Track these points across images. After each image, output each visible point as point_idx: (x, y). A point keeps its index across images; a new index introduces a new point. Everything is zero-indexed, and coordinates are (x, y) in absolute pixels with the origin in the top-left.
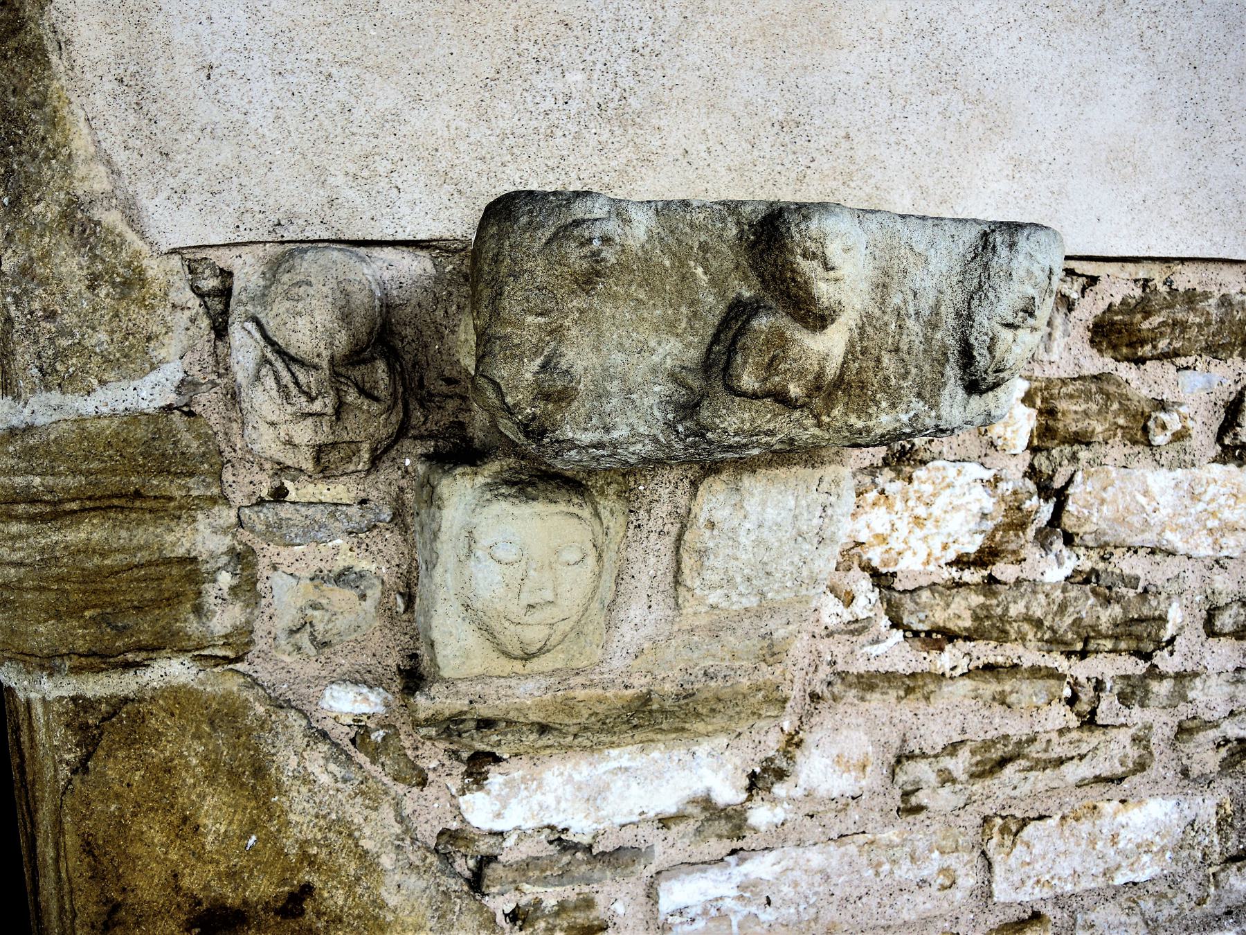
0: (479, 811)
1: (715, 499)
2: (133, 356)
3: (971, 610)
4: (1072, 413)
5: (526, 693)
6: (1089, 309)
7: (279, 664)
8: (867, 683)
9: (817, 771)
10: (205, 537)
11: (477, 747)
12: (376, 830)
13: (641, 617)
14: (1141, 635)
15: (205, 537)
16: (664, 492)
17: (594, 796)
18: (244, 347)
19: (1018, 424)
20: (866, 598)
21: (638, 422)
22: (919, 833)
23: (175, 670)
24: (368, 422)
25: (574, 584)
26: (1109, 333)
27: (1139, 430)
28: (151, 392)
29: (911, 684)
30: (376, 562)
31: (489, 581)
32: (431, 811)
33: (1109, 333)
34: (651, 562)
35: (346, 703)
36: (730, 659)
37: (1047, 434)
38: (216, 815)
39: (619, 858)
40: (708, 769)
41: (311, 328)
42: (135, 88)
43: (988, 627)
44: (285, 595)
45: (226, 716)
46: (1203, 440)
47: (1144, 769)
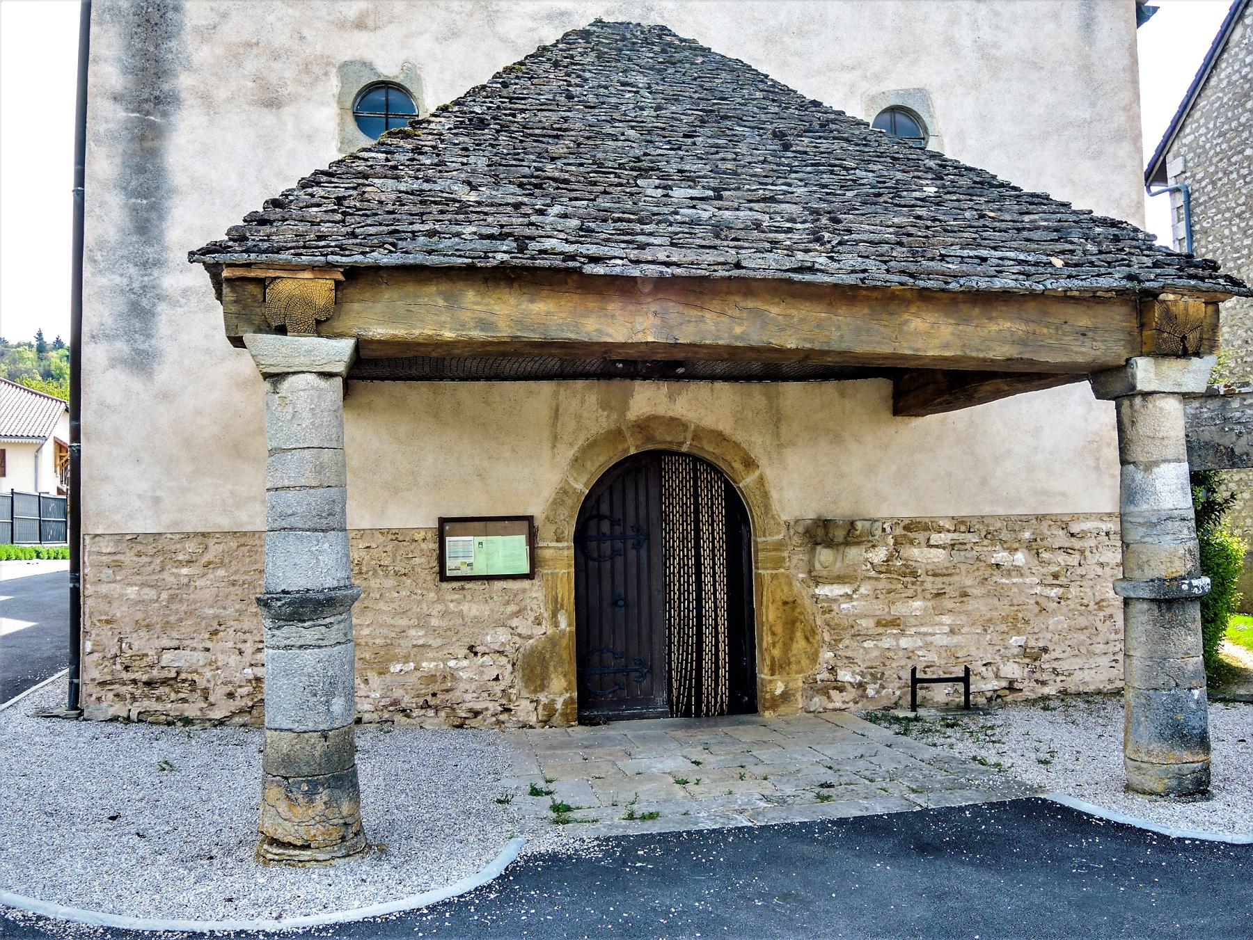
0: (817, 591)
1: (847, 550)
2: (778, 533)
3: (885, 568)
4: (900, 540)
5: (825, 573)
6: (902, 525)
7: (793, 571)
8: (870, 578)
9: (863, 590)
10: (786, 554)
11: (817, 581)
12: (804, 593)
13: (838, 564)
14: (914, 574)
15: (786, 554)
16: (841, 548)
17: (832, 591)
18: (792, 532)
19: (891, 541)
20: (869, 566)
21: (841, 539)
22: (879, 602)
23: (782, 570)
24: (806, 540)
25: (831, 559)
26: (906, 528)
27: (911, 542)
28: (781, 537)
29: (877, 579)
30: (805, 558)
31: (822, 558)
32: (811, 591)
33: (906, 528)
34: (840, 558)
35: (801, 576)
36: (849, 571)
37: (895, 544)
38: (786, 589)
39: (835, 600)
40: (847, 589)
41: (801, 530)
42: (780, 502)
43: (888, 572)
44: (794, 561)
45: (788, 576)
46: (923, 544)
47: (825, 524)
